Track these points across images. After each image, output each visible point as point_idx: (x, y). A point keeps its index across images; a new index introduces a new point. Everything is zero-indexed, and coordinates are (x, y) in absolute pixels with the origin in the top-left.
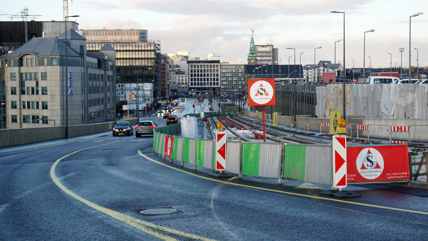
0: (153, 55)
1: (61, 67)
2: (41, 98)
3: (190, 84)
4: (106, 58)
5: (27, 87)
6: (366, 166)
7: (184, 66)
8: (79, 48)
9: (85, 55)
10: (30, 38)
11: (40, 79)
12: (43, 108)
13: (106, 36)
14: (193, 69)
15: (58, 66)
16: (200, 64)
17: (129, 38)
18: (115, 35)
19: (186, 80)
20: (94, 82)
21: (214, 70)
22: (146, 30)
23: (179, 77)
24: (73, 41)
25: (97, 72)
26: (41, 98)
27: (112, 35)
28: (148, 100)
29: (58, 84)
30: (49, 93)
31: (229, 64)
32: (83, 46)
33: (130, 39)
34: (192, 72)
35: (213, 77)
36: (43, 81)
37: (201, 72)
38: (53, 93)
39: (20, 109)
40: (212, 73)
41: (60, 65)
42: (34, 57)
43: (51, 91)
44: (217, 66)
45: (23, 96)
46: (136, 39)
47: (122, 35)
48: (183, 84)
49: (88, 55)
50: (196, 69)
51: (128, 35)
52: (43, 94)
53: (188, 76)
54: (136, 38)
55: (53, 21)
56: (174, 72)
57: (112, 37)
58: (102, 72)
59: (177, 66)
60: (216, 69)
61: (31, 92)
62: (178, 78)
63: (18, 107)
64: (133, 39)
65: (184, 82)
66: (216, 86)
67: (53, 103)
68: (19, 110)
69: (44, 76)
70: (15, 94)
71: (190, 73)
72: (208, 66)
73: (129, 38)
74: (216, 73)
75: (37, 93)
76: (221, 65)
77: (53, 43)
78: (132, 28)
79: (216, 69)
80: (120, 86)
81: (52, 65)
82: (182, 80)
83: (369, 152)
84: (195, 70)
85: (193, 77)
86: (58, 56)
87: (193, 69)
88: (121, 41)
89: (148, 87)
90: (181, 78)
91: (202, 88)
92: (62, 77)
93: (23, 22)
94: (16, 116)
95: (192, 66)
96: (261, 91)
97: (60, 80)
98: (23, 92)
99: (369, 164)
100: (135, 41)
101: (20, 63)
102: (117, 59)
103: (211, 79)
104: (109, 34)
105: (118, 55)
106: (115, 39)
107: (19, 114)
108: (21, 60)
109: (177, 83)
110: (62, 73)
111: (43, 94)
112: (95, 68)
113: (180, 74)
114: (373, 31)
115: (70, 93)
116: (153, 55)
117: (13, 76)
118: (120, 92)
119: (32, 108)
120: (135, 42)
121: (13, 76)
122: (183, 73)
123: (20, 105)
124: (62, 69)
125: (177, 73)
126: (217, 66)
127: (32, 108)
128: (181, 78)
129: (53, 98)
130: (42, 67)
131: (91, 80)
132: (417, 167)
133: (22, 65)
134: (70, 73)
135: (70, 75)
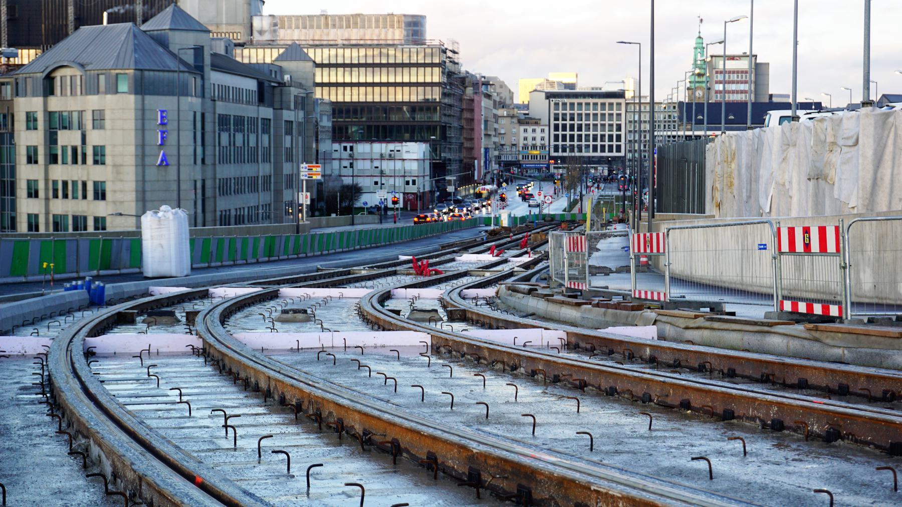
0: (435, 76)
1: (140, 97)
2: (90, 173)
3: (552, 150)
4: (287, 77)
5: (62, 147)
7: (541, 108)
9: (207, 69)
10: (76, 28)
11: (89, 124)
12: (96, 197)
13: (325, 31)
14: (560, 112)
15: (130, 93)
16: (576, 101)
17: (380, 35)
18: (348, 27)
19: (543, 139)
20: (239, 137)
21: (603, 115)
22: (421, 16)
23: (525, 131)
24: (177, 33)
25: (251, 111)
26: (90, 173)
27: (341, 27)
28: (414, 182)
29: (131, 137)
30: (108, 160)
31: (578, 90)
32: (203, 47)
33: (383, 37)
34: (556, 119)
35: (607, 133)
36: (96, 132)
37: (572, 119)
38: (119, 161)
39: (47, 199)
40: (607, 122)
41: (136, 93)
42: (77, 72)
43: (113, 156)
44: (619, 104)
45: (53, 167)
46: (397, 37)
47: (363, 27)
48: (534, 147)
49: (215, 67)
50: (568, 112)
51: (377, 27)
52: (96, 162)
53: (546, 129)
54: (397, 34)
56: (515, 120)
57: (340, 32)
58: (266, 112)
60: (615, 112)
61: (69, 158)
62: (522, 135)
63: (42, 194)
64: (390, 37)
65: (538, 144)
66: (615, 154)
67: (119, 186)
68: (43, 202)
69: (99, 120)
70: (36, 162)
71: (553, 122)
72: (595, 104)
73: (380, 35)
74: (615, 122)
75: (84, 162)
76: (627, 104)
77: (123, 38)
78: (390, 12)
79: (615, 112)
80: (345, 148)
81: (117, 92)
82: (534, 139)
84: (566, 114)
85: (560, 133)
86: (131, 71)
87: (560, 112)
88: (362, 42)
89: (414, 153)
90: (530, 135)
91: (580, 157)
92: (140, 122)
94: (37, 216)
95: (557, 104)
97: (136, 130)
98: (53, 159)
100: (396, 42)
101: (48, 87)
102: (318, 85)
103: (603, 136)
104: (334, 26)
105: (321, 76)
106: (346, 36)
107: (43, 211)
109: (521, 145)
110: (140, 113)
111: (96, 162)
112: (248, 103)
113: (527, 123)
115: (162, 161)
116: (435, 76)
118: (346, 163)
119: (73, 198)
120: (394, 45)
121: (31, 120)
122: (537, 122)
123: (47, 189)
124: (140, 102)
125: (520, 122)
126: (619, 104)
127: (73, 198)
128: (530, 135)
129: (118, 173)
131: (242, 131)
134: (162, 112)
135: (162, 117)
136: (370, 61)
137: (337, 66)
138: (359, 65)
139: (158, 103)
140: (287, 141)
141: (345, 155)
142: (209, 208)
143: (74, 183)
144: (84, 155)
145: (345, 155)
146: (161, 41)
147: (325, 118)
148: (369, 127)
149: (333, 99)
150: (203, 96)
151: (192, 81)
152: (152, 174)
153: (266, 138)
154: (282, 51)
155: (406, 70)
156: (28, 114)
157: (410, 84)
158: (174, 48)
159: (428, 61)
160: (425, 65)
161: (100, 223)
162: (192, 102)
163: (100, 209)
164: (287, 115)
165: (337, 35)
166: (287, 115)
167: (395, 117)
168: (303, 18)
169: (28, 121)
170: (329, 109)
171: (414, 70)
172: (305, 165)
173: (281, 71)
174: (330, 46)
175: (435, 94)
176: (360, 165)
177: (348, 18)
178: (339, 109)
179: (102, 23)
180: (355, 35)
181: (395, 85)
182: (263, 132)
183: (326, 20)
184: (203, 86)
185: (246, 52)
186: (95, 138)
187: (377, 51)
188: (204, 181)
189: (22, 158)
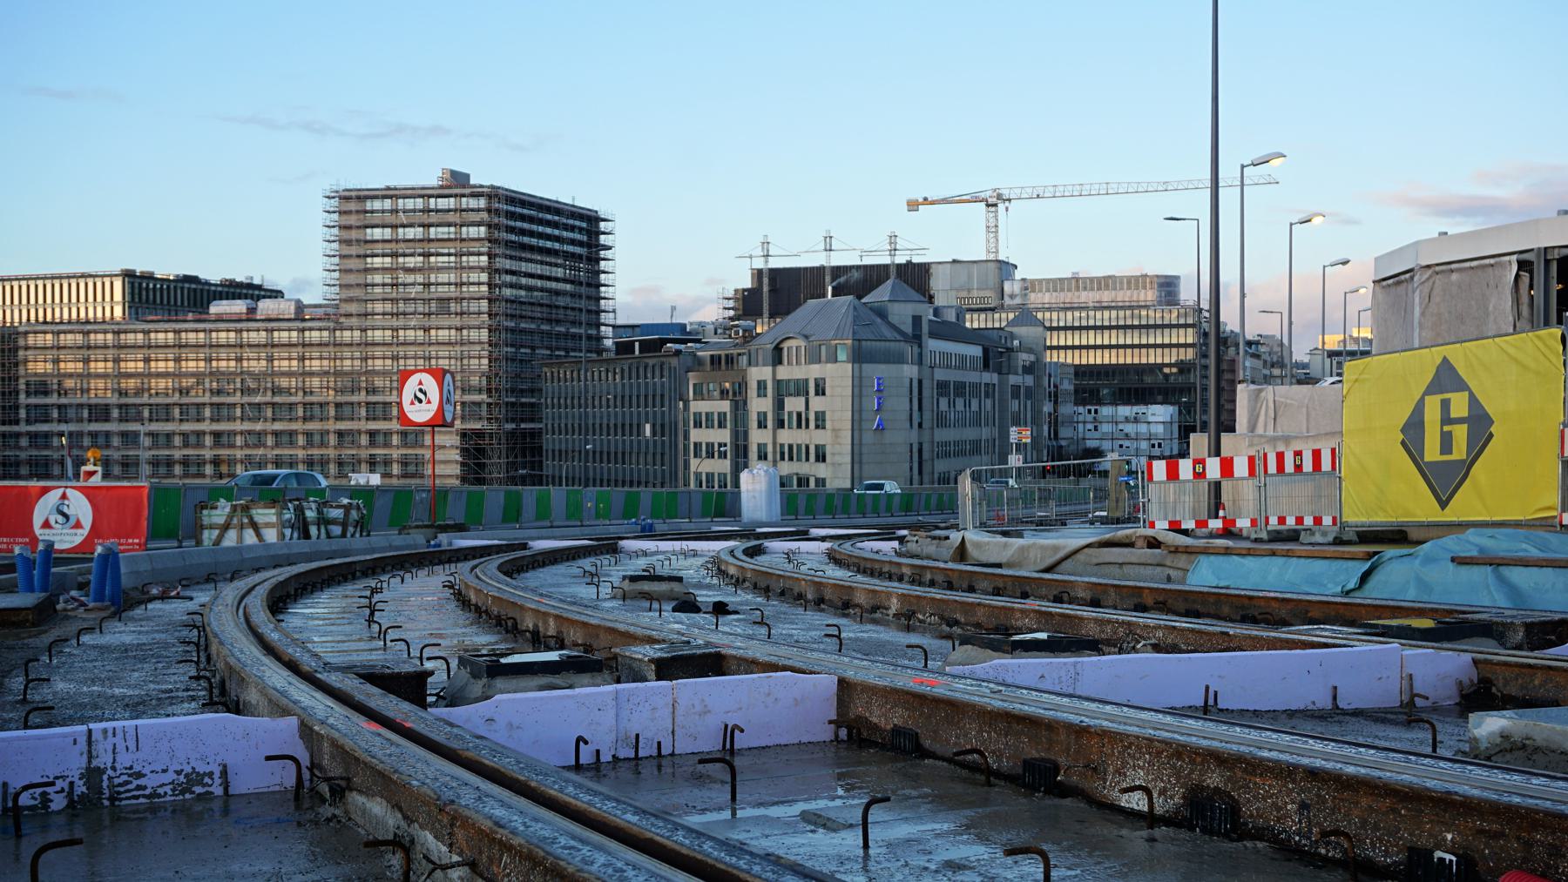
0: (1190, 337)
5: (816, 413)
6: (52, 522)
8: (910, 320)
9: (925, 337)
12: (817, 460)
18: (1099, 289)
20: (960, 402)
24: (896, 305)
25: (972, 377)
38: (837, 426)
39: (775, 462)
45: (780, 431)
49: (934, 335)
52: (817, 427)
54: (1150, 295)
55: (954, 261)
57: (1091, 294)
58: (990, 377)
59: (1305, 366)
63: (770, 456)
75: (807, 426)
81: (836, 361)
83: (64, 496)
93: (821, 269)
96: (421, 396)
98: (780, 424)
99: (60, 519)
101: (777, 357)
102: (1052, 348)
108: (778, 350)
111: (817, 427)
114: (1345, 263)
117: (761, 386)
118: (1091, 426)
121: (761, 386)
123: (774, 452)
130: (817, 366)
132: (216, 532)
133: (780, 362)
136: (1121, 323)
137: (1088, 328)
138: (1110, 328)
139: (874, 371)
140: (1014, 405)
141: (1090, 418)
142: (927, 468)
143: (799, 446)
144: (807, 420)
145: (1090, 418)
146: (881, 313)
147: (1066, 382)
148: (1121, 390)
149: (1077, 362)
150: (920, 363)
151: (909, 350)
152: (868, 437)
153: (989, 402)
154: (1011, 316)
155: (1159, 331)
156: (759, 382)
157: (1163, 346)
158: (893, 319)
159: (1182, 321)
160: (1178, 326)
161: (821, 482)
162: (910, 371)
163: (821, 470)
164: (1013, 379)
165: (1087, 297)
166: (1013, 379)
167: (1148, 379)
168: (1054, 281)
169: (759, 388)
170: (1072, 370)
171: (1167, 331)
172: (1014, 429)
173: (1012, 336)
174: (1081, 309)
175: (1190, 354)
176: (1106, 428)
177: (1099, 279)
178: (1081, 371)
179: (824, 295)
180: (1106, 296)
181: (1148, 346)
182: (987, 396)
183: (1077, 282)
184: (920, 355)
185: (997, 316)
186: (817, 404)
187: (1128, 313)
188: (921, 444)
189: (754, 424)
